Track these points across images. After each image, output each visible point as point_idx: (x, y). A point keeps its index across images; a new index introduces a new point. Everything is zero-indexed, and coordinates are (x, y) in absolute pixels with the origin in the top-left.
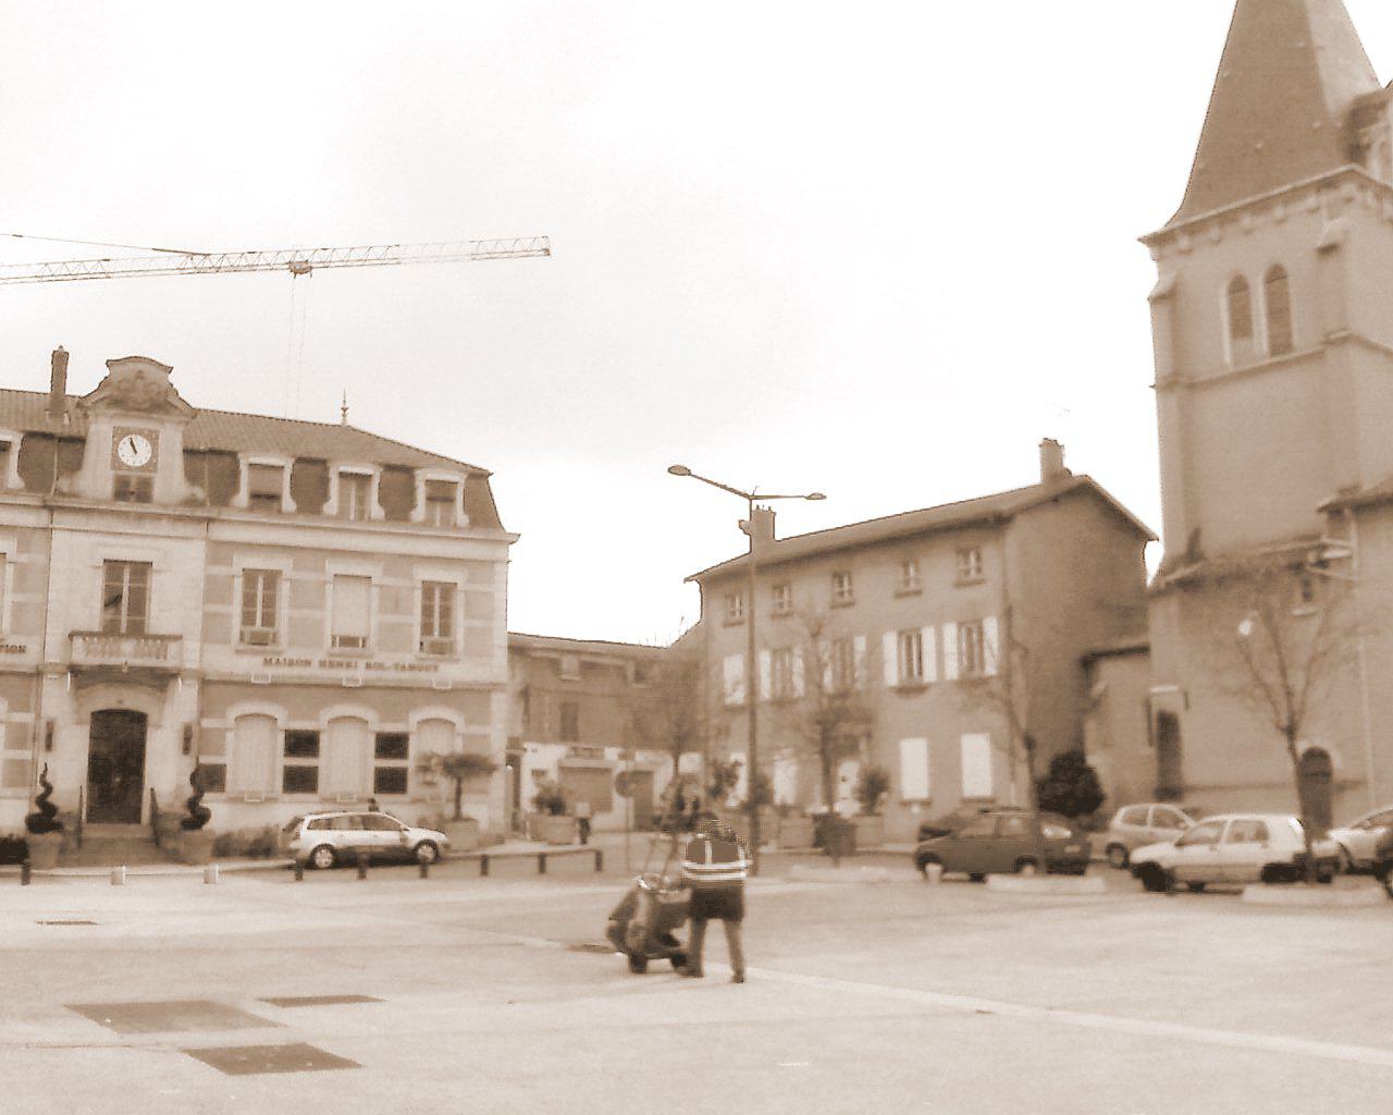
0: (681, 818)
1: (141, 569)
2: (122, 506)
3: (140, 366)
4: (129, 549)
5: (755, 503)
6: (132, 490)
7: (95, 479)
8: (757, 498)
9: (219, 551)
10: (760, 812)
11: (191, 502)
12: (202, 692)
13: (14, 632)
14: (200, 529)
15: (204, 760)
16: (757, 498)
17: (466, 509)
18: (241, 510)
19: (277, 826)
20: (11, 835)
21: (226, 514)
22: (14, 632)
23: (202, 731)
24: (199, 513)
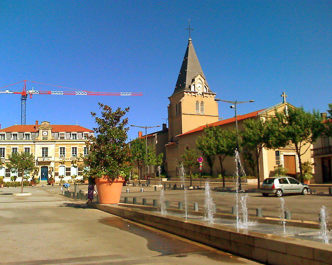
1: (47, 148)
3: (45, 122)
7: (40, 138)
12: (55, 163)
15: (56, 172)
23: (55, 168)
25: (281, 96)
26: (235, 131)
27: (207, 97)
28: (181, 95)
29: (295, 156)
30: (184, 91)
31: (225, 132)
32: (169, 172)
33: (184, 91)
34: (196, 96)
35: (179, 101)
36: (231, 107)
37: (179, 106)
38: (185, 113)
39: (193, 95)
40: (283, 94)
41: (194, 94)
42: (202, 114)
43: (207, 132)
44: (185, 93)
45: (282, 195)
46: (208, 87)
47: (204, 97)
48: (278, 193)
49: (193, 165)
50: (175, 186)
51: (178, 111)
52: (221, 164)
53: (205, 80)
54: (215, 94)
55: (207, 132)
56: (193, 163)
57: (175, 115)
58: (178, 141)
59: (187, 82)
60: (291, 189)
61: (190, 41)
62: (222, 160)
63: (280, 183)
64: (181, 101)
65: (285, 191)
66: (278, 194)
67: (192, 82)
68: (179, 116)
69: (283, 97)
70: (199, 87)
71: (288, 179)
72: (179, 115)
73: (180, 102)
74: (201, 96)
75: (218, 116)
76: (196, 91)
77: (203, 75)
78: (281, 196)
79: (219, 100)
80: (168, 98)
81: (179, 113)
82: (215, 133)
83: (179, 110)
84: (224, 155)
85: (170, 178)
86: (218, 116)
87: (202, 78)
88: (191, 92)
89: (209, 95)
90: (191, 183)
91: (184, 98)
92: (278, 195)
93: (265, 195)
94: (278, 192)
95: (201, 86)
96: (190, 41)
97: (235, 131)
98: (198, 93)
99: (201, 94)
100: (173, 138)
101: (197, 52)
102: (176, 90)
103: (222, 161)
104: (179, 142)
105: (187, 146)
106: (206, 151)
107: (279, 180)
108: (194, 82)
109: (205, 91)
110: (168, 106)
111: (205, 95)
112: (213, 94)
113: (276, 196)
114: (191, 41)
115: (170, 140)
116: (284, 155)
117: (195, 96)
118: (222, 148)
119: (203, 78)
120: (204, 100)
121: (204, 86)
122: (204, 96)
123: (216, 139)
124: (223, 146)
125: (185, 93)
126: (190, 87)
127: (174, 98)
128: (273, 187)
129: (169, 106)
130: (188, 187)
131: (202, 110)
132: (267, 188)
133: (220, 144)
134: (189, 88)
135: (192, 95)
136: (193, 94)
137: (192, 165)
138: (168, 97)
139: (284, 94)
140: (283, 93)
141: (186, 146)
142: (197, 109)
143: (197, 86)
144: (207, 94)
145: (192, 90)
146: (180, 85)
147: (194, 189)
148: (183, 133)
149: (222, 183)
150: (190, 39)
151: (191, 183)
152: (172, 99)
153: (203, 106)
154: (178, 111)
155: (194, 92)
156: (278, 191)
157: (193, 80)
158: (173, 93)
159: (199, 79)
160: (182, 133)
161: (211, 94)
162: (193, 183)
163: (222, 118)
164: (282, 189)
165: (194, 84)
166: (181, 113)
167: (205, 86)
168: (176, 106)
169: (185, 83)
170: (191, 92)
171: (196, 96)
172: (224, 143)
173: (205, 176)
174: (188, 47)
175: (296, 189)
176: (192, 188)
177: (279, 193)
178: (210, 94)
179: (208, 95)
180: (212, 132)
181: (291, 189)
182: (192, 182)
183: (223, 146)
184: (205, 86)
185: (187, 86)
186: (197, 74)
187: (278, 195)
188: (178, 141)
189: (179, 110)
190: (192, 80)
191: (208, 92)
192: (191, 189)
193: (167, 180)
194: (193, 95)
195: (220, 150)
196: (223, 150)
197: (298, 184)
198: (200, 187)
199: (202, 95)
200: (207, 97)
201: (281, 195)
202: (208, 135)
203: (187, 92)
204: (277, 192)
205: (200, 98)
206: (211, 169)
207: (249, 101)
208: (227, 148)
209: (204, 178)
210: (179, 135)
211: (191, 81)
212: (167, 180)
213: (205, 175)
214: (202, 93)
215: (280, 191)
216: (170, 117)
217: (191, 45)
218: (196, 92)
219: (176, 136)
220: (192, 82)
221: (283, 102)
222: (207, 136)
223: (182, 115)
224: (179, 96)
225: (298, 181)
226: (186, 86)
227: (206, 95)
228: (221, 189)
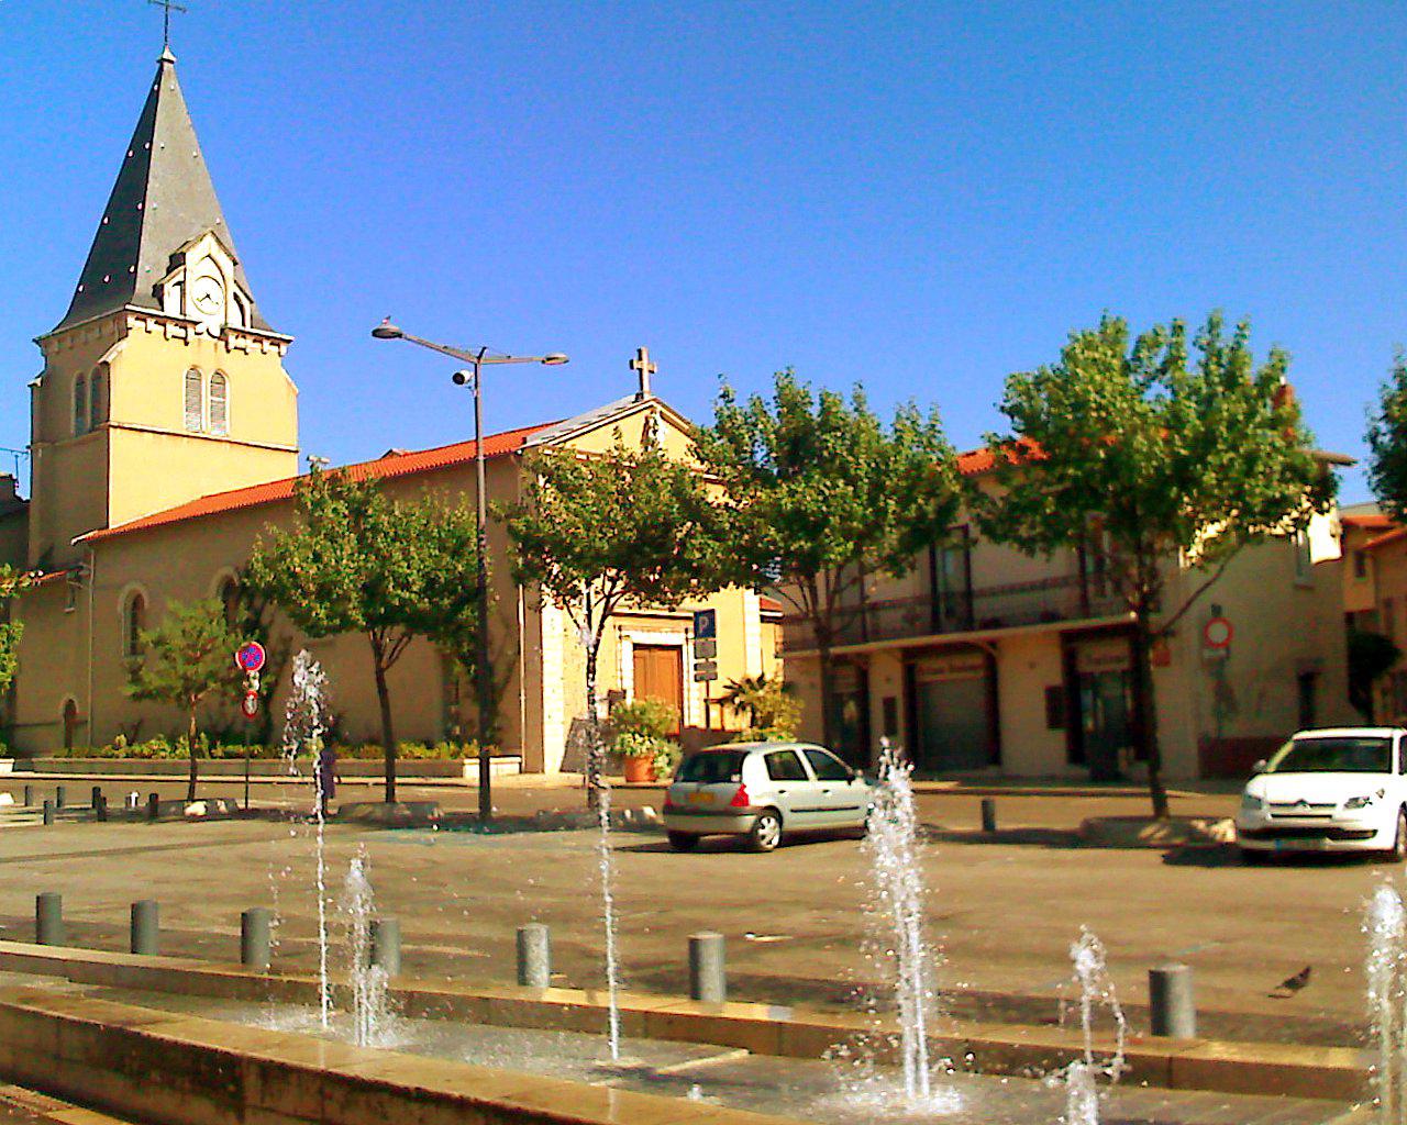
25: (632, 367)
26: (464, 511)
27: (246, 354)
28: (110, 327)
29: (678, 648)
30: (128, 307)
31: (407, 510)
32: (26, 725)
33: (128, 307)
34: (187, 344)
35: (102, 360)
36: (459, 379)
37: (96, 390)
38: (127, 421)
39: (174, 337)
40: (640, 359)
41: (182, 333)
42: (215, 434)
43: (318, 504)
44: (131, 321)
45: (781, 839)
46: (251, 302)
47: (228, 351)
48: (761, 832)
49: (212, 685)
50: (98, 798)
51: (89, 406)
52: (380, 680)
53: (235, 264)
54: (289, 341)
55: (318, 504)
56: (212, 675)
57: (72, 430)
58: (81, 568)
59: (143, 265)
60: (820, 810)
61: (166, 65)
62: (385, 658)
63: (772, 778)
64: (109, 357)
65: (794, 822)
66: (763, 837)
67: (169, 271)
68: (96, 439)
69: (641, 370)
70: (208, 296)
71: (805, 751)
72: (93, 429)
73: (106, 363)
74: (216, 345)
75: (297, 452)
76: (192, 315)
77: (227, 240)
78: (776, 847)
79: (400, 336)
80: (34, 340)
81: (95, 419)
82: (358, 512)
83: (96, 402)
84: (399, 629)
85: (33, 760)
86: (297, 452)
87: (223, 253)
88: (161, 321)
89: (258, 345)
90: (193, 781)
91: (122, 345)
92: (764, 843)
93: (684, 843)
94: (763, 827)
95: (217, 293)
96: (166, 65)
97: (464, 511)
98: (199, 328)
99: (217, 333)
100: (52, 548)
101: (199, 126)
102: (80, 303)
103: (383, 665)
104: (89, 569)
105: (131, 592)
106: (310, 609)
107: (767, 758)
108: (182, 268)
109: (235, 322)
110: (35, 384)
111: (232, 338)
112: (276, 342)
113: (748, 844)
114: (172, 62)
115: (34, 559)
116: (636, 646)
117: (182, 341)
118: (397, 595)
119: (229, 255)
120: (232, 363)
121: (231, 297)
122: (231, 346)
123: (364, 545)
124: (406, 586)
125: (131, 321)
126: (158, 292)
127: (68, 343)
128: (741, 798)
129: (38, 381)
130: (181, 804)
131: (218, 414)
132: (703, 806)
133: (393, 573)
134: (153, 295)
135: (169, 336)
136: (172, 329)
137: (203, 687)
138: (36, 337)
139: (644, 355)
140: (640, 351)
141: (127, 588)
142: (193, 406)
143: (195, 289)
144: (244, 337)
145: (171, 307)
146: (106, 280)
147: (212, 815)
148: (111, 527)
149: (384, 780)
150: (167, 55)
151: (193, 781)
152: (55, 347)
153: (224, 398)
154: (89, 406)
155: (182, 317)
156: (764, 821)
157: (177, 260)
158: (62, 319)
159: (209, 256)
160: (108, 527)
161: (268, 338)
162: (404, 784)
163: (323, 459)
164: (780, 808)
165: (180, 278)
166: (108, 420)
167: (236, 297)
168: (81, 381)
169: (132, 269)
170: (162, 321)
171: (187, 344)
172: (412, 566)
173: (230, 748)
174: (154, 97)
175: (846, 809)
176: (198, 808)
177: (770, 830)
178: (259, 339)
179: (248, 343)
180: (342, 507)
181: (820, 810)
182: (398, 780)
183: (406, 586)
184: (236, 297)
185: (143, 286)
186: (197, 229)
187: (764, 843)
188: (81, 568)
189: (96, 402)
190: (171, 257)
191: (248, 329)
192: (194, 818)
193: (13, 770)
194: (174, 337)
195: (386, 603)
196: (403, 602)
197: (850, 779)
198: (241, 806)
199: (219, 338)
200: (246, 354)
201: (776, 841)
202: (320, 519)
203: (142, 317)
204: (758, 825)
205: (207, 354)
206: (267, 712)
207: (543, 357)
208: (422, 593)
209: (229, 755)
210: (91, 534)
211: (166, 263)
212: (13, 770)
213: (235, 743)
214: (222, 330)
215: (773, 820)
216: (44, 436)
217: (170, 83)
218: (187, 318)
219: (74, 541)
220: (169, 271)
221: (639, 396)
222: (314, 525)
223: (111, 430)
224: (96, 333)
225: (849, 770)
226: (137, 286)
227: (241, 342)
228: (379, 813)
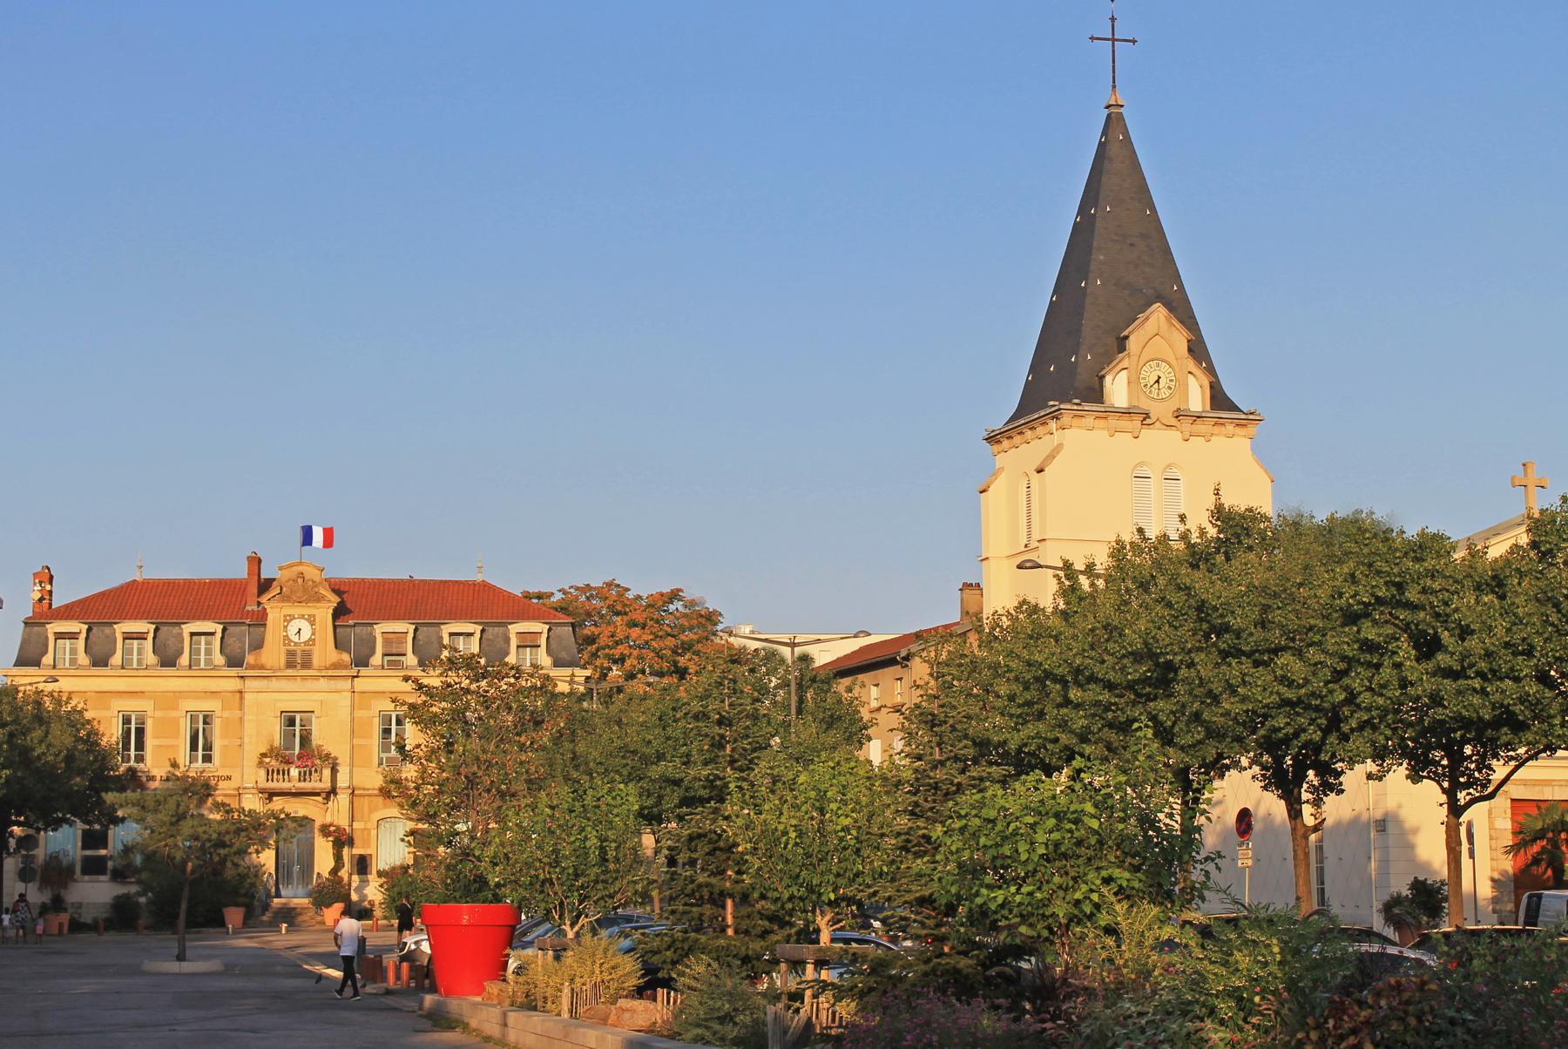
0: (1438, 615)
2: (290, 672)
4: (294, 703)
5: (797, 650)
6: (298, 660)
7: (273, 654)
8: (799, 644)
9: (360, 699)
10: (1066, 419)
11: (335, 666)
13: (223, 766)
14: (347, 684)
16: (799, 644)
17: (549, 652)
18: (376, 667)
19: (381, 886)
20: (1280, 797)
21: (364, 671)
22: (223, 766)
24: (344, 673)
